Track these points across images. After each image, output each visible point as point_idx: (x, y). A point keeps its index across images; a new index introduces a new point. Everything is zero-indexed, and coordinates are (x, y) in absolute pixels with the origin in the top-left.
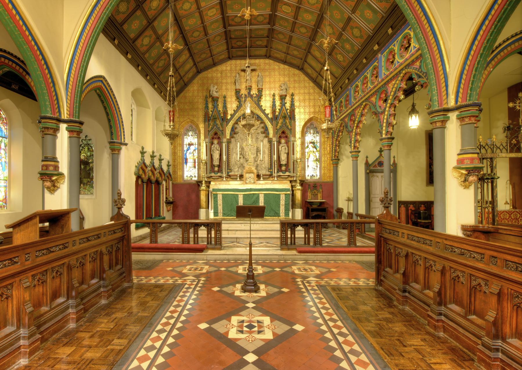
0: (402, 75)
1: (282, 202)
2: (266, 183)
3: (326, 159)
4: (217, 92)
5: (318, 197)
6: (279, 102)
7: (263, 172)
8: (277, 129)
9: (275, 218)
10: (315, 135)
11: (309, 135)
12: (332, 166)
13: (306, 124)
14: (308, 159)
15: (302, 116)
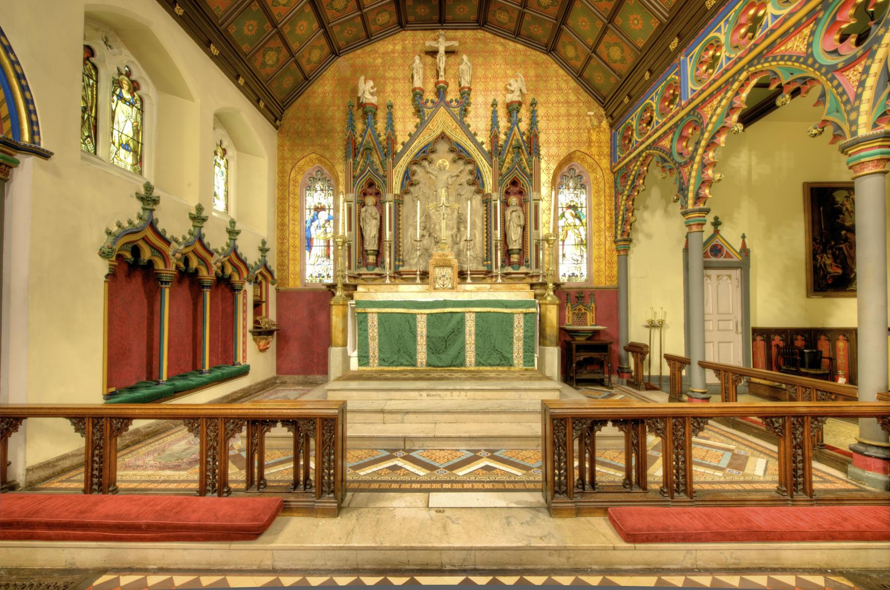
0: (641, 159)
1: (518, 332)
2: (478, 290)
3: (603, 239)
4: (372, 94)
5: (585, 319)
6: (505, 120)
7: (469, 266)
8: (501, 175)
9: (500, 368)
10: (578, 192)
11: (566, 191)
12: (615, 253)
13: (560, 167)
14: (563, 241)
15: (554, 150)
